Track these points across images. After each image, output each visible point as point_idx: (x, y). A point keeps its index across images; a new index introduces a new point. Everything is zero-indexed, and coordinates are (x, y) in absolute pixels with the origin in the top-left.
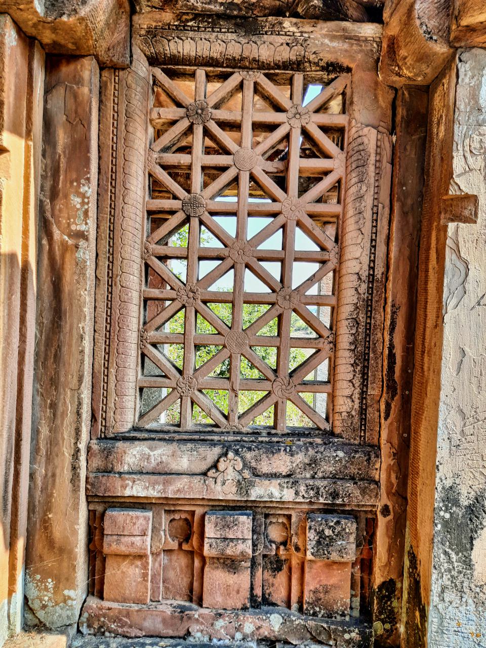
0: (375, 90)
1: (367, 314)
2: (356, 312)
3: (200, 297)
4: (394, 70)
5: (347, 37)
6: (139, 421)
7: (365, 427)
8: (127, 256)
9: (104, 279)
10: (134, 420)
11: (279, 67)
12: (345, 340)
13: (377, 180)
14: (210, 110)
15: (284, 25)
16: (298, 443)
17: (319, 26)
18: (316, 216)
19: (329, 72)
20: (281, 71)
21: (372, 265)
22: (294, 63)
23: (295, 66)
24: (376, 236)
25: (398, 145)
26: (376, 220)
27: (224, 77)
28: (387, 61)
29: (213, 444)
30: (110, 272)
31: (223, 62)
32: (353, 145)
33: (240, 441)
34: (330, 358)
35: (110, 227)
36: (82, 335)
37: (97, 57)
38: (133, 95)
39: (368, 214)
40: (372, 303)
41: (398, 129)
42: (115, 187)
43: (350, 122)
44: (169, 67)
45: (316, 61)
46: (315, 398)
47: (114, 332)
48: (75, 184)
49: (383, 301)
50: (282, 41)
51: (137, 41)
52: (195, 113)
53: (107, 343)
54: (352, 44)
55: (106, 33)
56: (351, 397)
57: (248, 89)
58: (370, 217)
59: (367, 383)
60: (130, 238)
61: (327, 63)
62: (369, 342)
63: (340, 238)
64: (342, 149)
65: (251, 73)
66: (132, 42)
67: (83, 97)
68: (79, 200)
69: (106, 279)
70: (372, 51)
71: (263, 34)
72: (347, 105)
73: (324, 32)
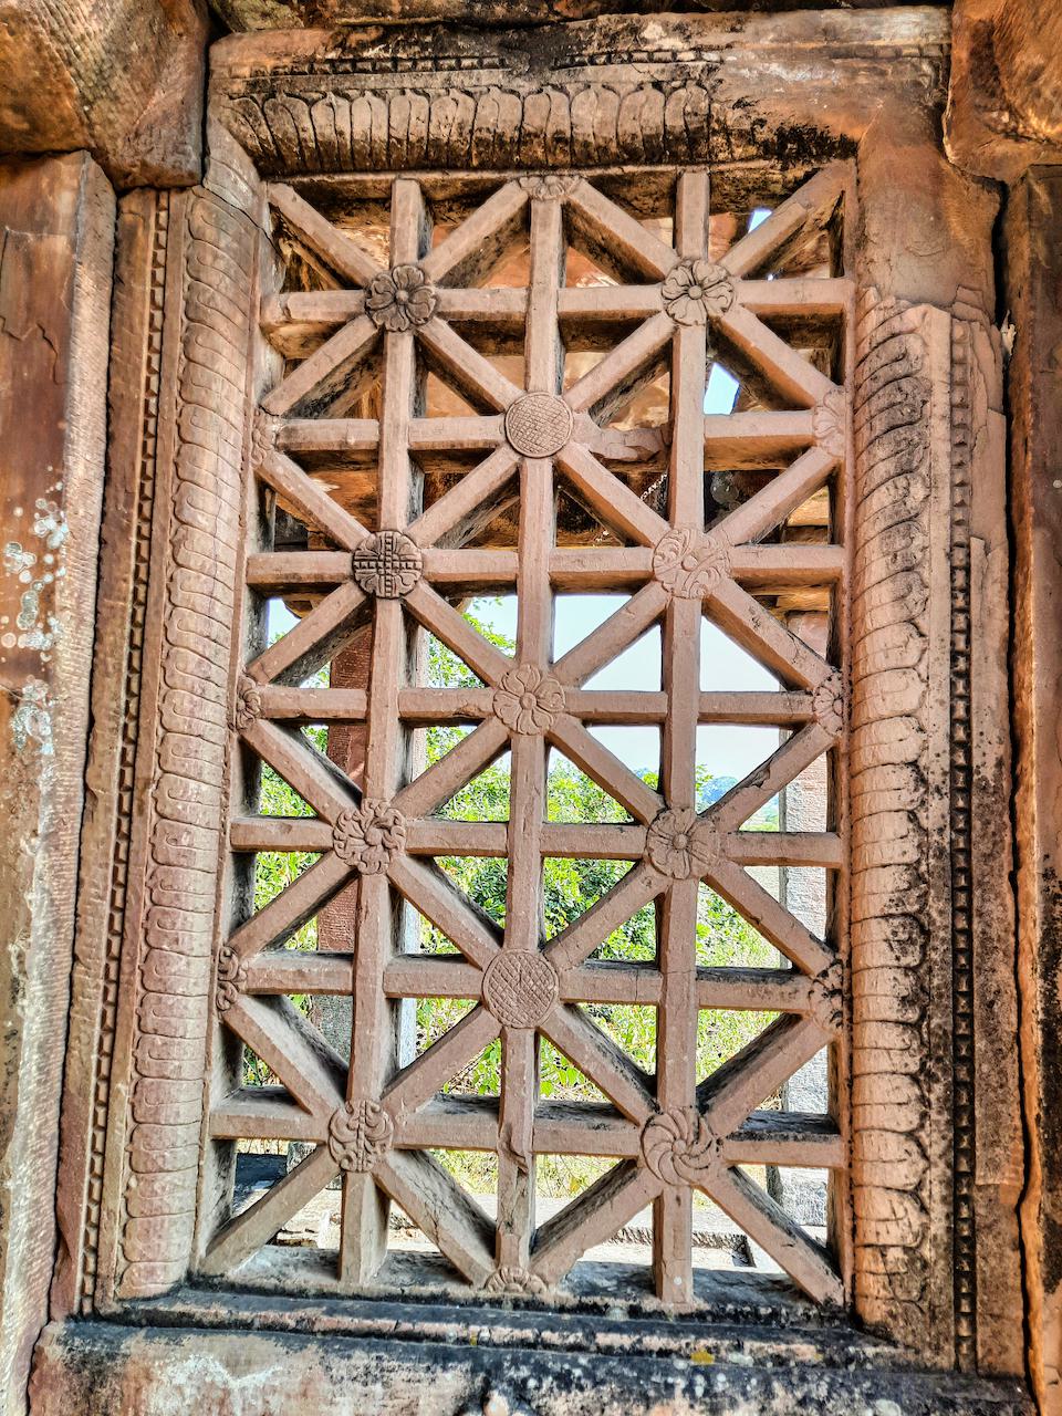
0: (936, 195)
1: (953, 899)
2: (916, 893)
3: (403, 843)
4: (997, 121)
5: (837, 52)
6: (209, 1251)
7: (973, 1304)
8: (179, 722)
9: (110, 792)
10: (194, 1250)
11: (633, 157)
12: (883, 991)
13: (960, 465)
14: (434, 289)
15: (646, 34)
16: (735, 1357)
17: (750, 28)
18: (762, 586)
19: (786, 161)
20: (639, 168)
21: (960, 734)
22: (678, 139)
23: (683, 148)
24: (968, 642)
25: (1023, 352)
26: (966, 591)
27: (475, 197)
28: (973, 97)
29: (442, 1356)
30: (128, 771)
31: (469, 153)
32: (874, 362)
33: (533, 1345)
34: (834, 1049)
35: (132, 634)
36: (15, 980)
37: (99, 154)
38: (209, 259)
39: (937, 572)
40: (968, 860)
41: (1020, 306)
42: (150, 521)
43: (859, 298)
44: (316, 179)
45: (747, 126)
46: (784, 881)
47: (133, 961)
48: (19, 512)
49: (1005, 858)
50: (639, 78)
51: (223, 111)
52: (394, 300)
53: (111, 998)
54: (855, 73)
55: (120, 82)
56: (915, 1193)
57: (545, 225)
58: (945, 581)
59: (972, 1142)
60: (191, 667)
61: (780, 133)
62: (969, 995)
63: (846, 648)
64: (837, 377)
65: (551, 179)
66: (210, 114)
67: (52, 268)
68: (28, 559)
69: (115, 792)
70: (918, 84)
71: (582, 64)
72: (846, 253)
73: (766, 42)
